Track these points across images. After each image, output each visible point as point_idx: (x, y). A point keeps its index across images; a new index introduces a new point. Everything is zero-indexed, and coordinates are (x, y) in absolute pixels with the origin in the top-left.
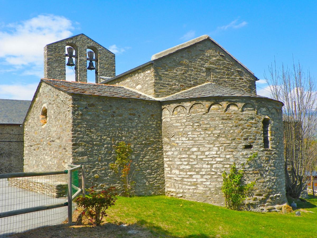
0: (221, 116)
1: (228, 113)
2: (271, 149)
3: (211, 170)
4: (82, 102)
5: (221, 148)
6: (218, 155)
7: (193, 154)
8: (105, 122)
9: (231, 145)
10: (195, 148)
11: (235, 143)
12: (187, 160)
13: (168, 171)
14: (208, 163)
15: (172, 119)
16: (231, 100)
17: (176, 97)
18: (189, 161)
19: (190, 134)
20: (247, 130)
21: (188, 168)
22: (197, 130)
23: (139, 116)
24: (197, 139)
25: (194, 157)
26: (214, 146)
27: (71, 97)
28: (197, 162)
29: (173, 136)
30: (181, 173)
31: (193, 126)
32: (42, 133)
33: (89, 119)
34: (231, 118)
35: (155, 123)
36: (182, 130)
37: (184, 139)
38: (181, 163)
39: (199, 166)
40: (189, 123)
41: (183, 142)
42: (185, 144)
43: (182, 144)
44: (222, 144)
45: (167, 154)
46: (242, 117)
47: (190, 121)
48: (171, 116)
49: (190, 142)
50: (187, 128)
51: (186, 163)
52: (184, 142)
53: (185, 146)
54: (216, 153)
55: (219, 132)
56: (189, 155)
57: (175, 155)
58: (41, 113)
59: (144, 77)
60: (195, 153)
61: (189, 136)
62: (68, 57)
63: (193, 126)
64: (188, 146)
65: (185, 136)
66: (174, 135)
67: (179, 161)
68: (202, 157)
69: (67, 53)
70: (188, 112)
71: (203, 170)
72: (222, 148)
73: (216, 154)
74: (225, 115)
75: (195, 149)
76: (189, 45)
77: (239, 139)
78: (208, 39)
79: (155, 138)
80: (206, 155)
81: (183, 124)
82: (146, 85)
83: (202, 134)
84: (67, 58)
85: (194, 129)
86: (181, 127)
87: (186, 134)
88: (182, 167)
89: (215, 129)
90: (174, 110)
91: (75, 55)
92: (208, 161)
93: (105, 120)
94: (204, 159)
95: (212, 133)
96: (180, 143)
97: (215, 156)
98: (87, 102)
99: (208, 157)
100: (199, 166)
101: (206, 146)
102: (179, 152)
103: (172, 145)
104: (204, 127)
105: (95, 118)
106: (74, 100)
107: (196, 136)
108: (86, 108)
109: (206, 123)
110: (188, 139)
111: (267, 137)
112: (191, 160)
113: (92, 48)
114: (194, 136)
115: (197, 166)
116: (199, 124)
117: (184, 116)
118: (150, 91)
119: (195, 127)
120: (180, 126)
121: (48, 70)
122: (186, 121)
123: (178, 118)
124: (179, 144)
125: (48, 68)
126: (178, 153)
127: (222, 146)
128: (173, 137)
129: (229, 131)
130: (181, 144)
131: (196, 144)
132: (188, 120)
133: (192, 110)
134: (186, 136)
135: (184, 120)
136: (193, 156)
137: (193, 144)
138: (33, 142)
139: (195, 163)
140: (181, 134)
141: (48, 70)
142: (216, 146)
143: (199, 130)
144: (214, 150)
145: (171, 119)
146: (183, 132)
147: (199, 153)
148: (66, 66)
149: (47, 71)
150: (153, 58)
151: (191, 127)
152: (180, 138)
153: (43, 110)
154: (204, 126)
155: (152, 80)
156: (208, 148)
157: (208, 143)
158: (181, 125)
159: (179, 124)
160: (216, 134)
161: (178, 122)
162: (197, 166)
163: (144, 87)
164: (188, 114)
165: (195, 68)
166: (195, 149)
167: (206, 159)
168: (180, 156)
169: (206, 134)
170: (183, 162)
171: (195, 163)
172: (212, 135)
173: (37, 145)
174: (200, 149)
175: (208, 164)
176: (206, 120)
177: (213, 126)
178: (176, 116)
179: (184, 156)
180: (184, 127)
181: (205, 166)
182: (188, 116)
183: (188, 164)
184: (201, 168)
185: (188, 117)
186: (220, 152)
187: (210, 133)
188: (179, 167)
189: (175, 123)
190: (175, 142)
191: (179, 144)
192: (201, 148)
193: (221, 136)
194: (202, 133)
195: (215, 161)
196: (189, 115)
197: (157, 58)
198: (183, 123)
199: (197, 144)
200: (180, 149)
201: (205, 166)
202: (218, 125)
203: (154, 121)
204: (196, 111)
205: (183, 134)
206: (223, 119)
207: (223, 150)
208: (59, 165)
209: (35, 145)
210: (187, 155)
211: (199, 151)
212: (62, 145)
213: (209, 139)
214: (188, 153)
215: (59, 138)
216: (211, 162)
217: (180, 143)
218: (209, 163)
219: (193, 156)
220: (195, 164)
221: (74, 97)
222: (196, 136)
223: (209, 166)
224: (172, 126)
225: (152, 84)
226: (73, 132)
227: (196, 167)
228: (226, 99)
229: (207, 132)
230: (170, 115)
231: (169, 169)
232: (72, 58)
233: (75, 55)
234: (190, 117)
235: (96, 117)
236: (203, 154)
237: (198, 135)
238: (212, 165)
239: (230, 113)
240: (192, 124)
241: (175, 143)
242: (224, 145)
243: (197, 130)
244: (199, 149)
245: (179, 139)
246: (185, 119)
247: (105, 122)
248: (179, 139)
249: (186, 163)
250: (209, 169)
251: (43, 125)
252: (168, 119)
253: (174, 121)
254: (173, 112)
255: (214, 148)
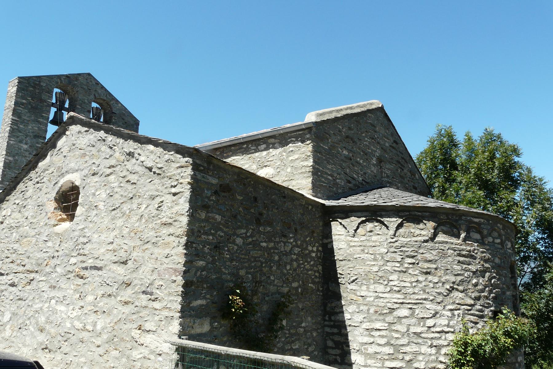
0: (457, 248)
3: (437, 358)
4: (210, 176)
5: (456, 313)
6: (451, 327)
7: (401, 323)
10: (406, 310)
12: (385, 334)
13: (336, 355)
14: (432, 344)
15: (352, 244)
16: (472, 219)
17: (362, 201)
19: (396, 279)
21: (387, 353)
22: (410, 271)
23: (296, 230)
24: (411, 290)
25: (403, 329)
27: (190, 160)
28: (408, 339)
29: (354, 281)
30: (369, 362)
31: (401, 262)
32: (50, 244)
33: (220, 223)
34: (473, 254)
35: (315, 249)
36: (375, 269)
37: (380, 288)
38: (372, 340)
39: (413, 348)
40: (393, 255)
41: (377, 294)
42: (382, 300)
43: (375, 299)
44: (459, 306)
45: (333, 318)
47: (396, 252)
48: (348, 238)
49: (394, 297)
50: (389, 266)
51: (383, 341)
52: (381, 295)
53: (383, 305)
54: (447, 324)
56: (390, 324)
57: (354, 323)
58: (54, 195)
59: (284, 154)
60: (404, 320)
61: (392, 283)
62: (55, 110)
63: (401, 262)
64: (389, 305)
65: (381, 281)
66: (356, 279)
67: (365, 336)
68: (419, 330)
69: (54, 101)
70: (392, 232)
71: (420, 358)
73: (448, 326)
75: (403, 312)
76: (332, 116)
78: (381, 110)
80: (429, 325)
81: (380, 258)
82: (289, 170)
83: (421, 282)
84: (53, 110)
85: (404, 270)
86: (373, 263)
87: (384, 279)
88: (372, 349)
90: (358, 228)
91: (67, 107)
93: (245, 230)
94: (423, 335)
96: (371, 297)
97: (446, 329)
98: (219, 178)
99: (432, 330)
100: (413, 348)
102: (366, 316)
103: (349, 299)
104: (425, 267)
105: (230, 222)
106: (195, 167)
107: (409, 285)
108: (216, 193)
110: (388, 289)
112: (396, 335)
113: (102, 102)
114: (403, 284)
115: (407, 349)
116: (414, 261)
117: (382, 240)
118: (299, 181)
119: (406, 265)
120: (370, 261)
121: (11, 124)
122: (386, 251)
123: (368, 244)
124: (368, 299)
125: (12, 119)
126: (364, 318)
127: (459, 309)
128: (352, 282)
130: (372, 299)
131: (408, 302)
132: (392, 250)
133: (401, 231)
134: (386, 283)
135: (381, 249)
136: (398, 327)
137: (401, 301)
138: (11, 265)
139: (404, 341)
140: (374, 277)
141: (11, 124)
143: (415, 273)
144: (443, 318)
145: (348, 245)
146: (380, 274)
147: (414, 321)
148: (49, 124)
149: (10, 125)
150: (311, 118)
151: (398, 265)
152: (372, 287)
153: (60, 188)
154: (426, 265)
155: (306, 160)
156: (433, 312)
158: (375, 260)
159: (370, 256)
161: (366, 251)
162: (407, 349)
163: (282, 172)
164: (392, 238)
166: (403, 312)
167: (427, 335)
168: (368, 324)
169: (430, 282)
170: (376, 339)
171: (404, 341)
172: (441, 284)
173: (26, 275)
174: (415, 313)
175: (431, 346)
176: (429, 254)
177: (443, 268)
178: (363, 238)
179: (378, 325)
180: (381, 263)
181: (424, 349)
182: (392, 243)
183: (388, 344)
184: (416, 354)
185: (392, 244)
186: (455, 322)
187: (436, 280)
188: (365, 349)
189: (358, 254)
190: (358, 294)
191: (368, 299)
192: (417, 312)
193: (457, 290)
195: (445, 339)
196: (394, 240)
197: (319, 120)
198: (379, 254)
199: (410, 301)
200: (369, 310)
201: (424, 349)
203: (314, 246)
204: (409, 232)
205: (378, 278)
209: (16, 273)
210: (387, 325)
211: (412, 315)
212: (136, 282)
214: (389, 319)
215: (125, 263)
216: (438, 342)
217: (371, 297)
218: (434, 344)
219: (398, 327)
220: (403, 345)
221: (197, 161)
222: (409, 285)
223: (433, 351)
224: (351, 259)
225: (308, 169)
226: (463, 235)
227: (405, 351)
228: (465, 216)
230: (346, 236)
231: (338, 352)
232: (63, 111)
233: (67, 107)
234: (397, 244)
235: (231, 219)
236: (422, 323)
237: (411, 283)
238: (438, 348)
240: (400, 260)
241: (357, 295)
243: (410, 271)
244: (414, 312)
245: (368, 288)
246: (385, 246)
248: (368, 288)
249: (383, 341)
250: (433, 357)
251: (57, 225)
252: (343, 243)
253: (358, 248)
254: (356, 231)
255: (444, 312)
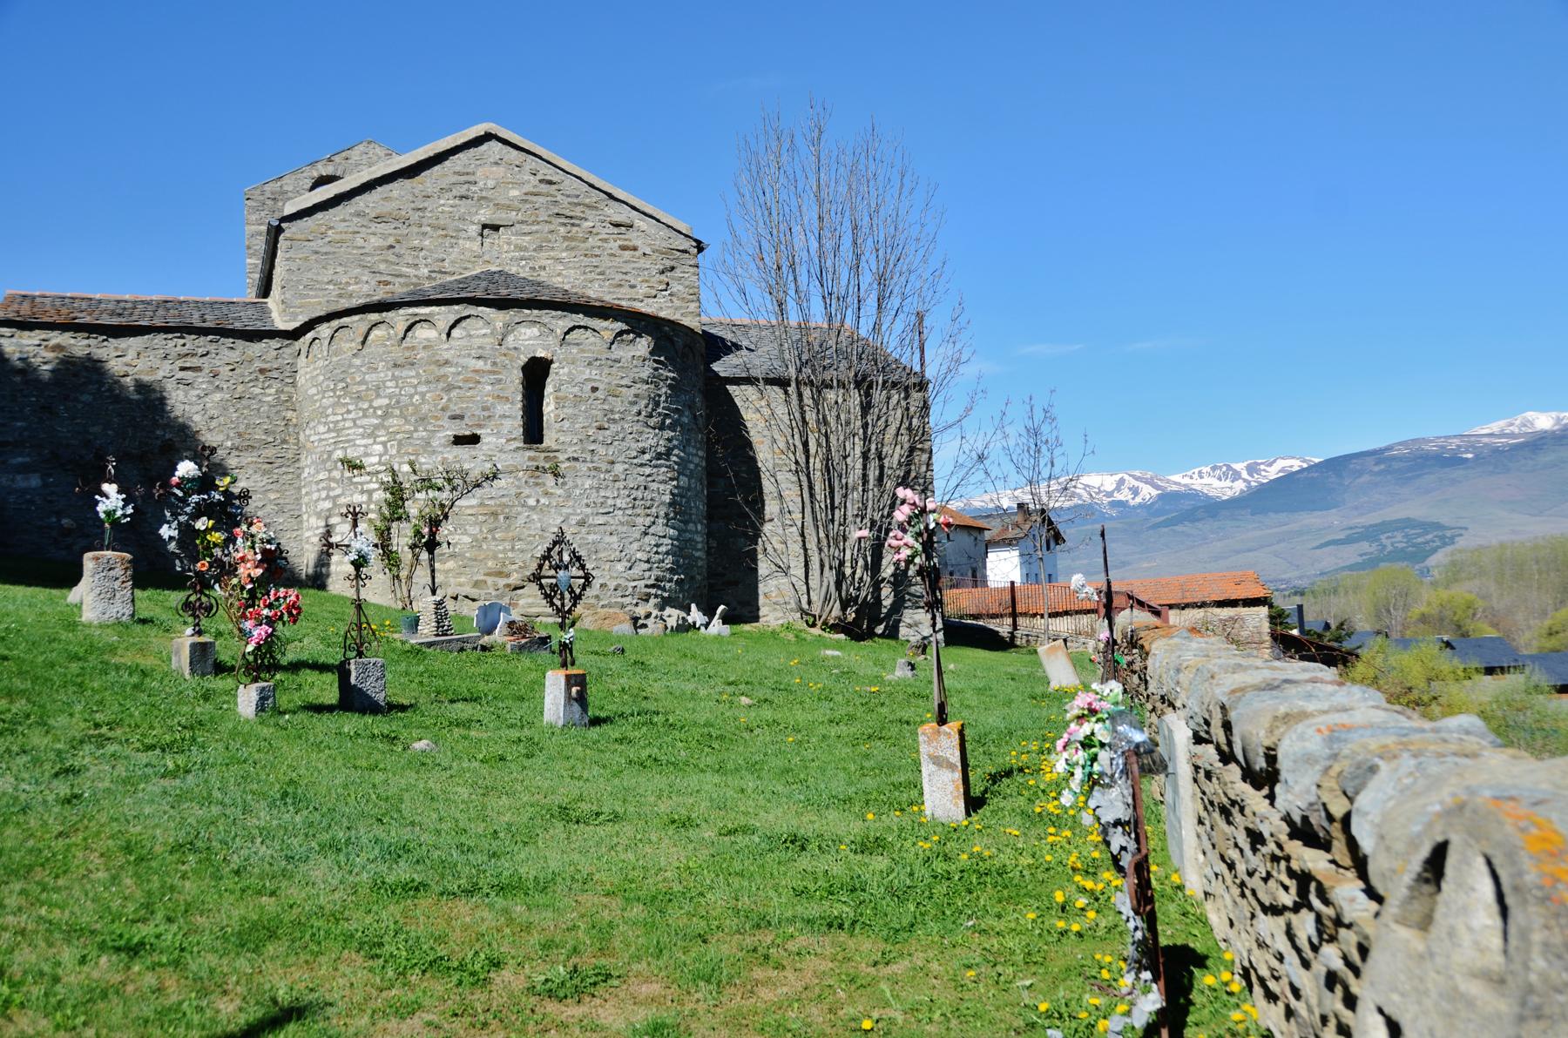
1: (408, 348)
2: (555, 447)
8: (99, 389)
9: (415, 435)
11: (425, 430)
18: (329, 489)
20: (462, 392)
26: (375, 442)
46: (447, 355)
55: (386, 401)
72: (392, 446)
73: (380, 463)
74: (398, 354)
77: (437, 418)
79: (266, 432)
89: (378, 396)
92: (362, 484)
95: (371, 406)
101: (358, 442)
109: (358, 379)
111: (869, 450)
129: (412, 396)
142: (379, 440)
157: (363, 436)
160: (380, 408)
165: (435, 228)
175: (362, 492)
187: (366, 406)
194: (351, 407)
202: (384, 382)
206: (395, 365)
207: (394, 452)
208: (951, 766)
213: (365, 422)
229: (360, 405)
239: (413, 348)
242: (398, 437)
247: (99, 389)
